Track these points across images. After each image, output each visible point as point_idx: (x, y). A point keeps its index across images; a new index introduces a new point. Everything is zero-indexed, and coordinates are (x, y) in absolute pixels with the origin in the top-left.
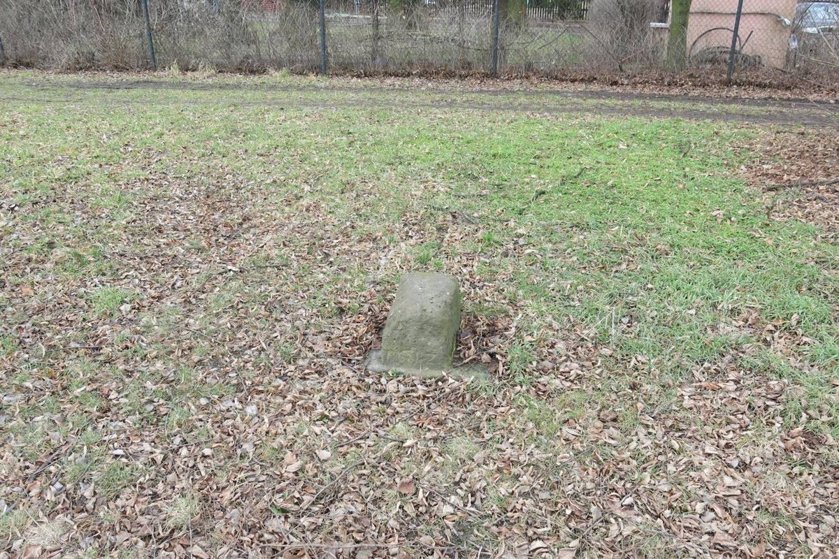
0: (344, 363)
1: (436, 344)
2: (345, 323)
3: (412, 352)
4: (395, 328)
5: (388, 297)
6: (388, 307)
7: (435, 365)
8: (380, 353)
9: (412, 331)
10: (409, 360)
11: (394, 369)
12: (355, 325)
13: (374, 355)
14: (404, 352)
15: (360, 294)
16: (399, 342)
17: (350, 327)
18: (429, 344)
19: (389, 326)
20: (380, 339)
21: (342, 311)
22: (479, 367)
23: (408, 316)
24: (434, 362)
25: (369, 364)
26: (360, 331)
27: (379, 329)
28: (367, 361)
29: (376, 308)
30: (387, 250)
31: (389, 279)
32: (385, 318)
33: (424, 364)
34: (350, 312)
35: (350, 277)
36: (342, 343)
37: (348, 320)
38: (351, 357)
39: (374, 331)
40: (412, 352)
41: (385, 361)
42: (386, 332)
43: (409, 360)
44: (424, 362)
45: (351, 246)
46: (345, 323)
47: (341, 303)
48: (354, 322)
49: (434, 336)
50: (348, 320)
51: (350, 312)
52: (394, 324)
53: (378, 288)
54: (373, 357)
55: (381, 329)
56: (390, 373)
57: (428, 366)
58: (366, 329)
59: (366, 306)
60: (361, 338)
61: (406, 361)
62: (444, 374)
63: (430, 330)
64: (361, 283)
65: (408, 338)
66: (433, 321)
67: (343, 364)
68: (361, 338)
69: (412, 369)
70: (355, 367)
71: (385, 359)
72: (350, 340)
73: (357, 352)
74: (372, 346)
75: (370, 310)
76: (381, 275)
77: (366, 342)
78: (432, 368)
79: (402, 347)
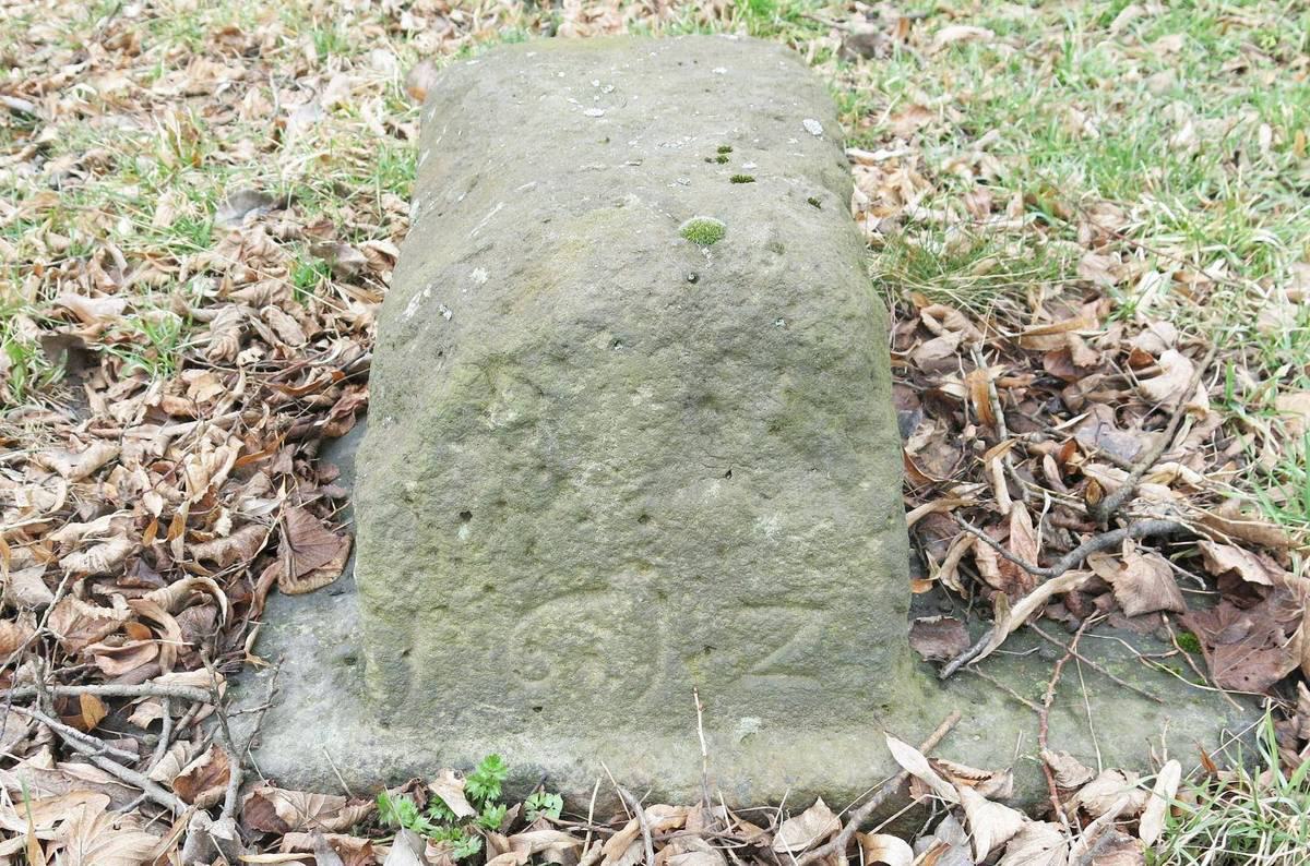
0: (70, 734)
1: (832, 521)
2: (105, 429)
3: (616, 603)
4: (460, 424)
5: (353, 256)
6: (358, 311)
7: (820, 689)
8: (349, 618)
9: (623, 410)
10: (595, 673)
11: (473, 747)
12: (158, 436)
13: (300, 637)
14: (548, 612)
15: (185, 261)
16: (504, 535)
17: (131, 450)
18: (770, 523)
19: (399, 409)
20: (331, 510)
21: (82, 360)
22: (1117, 654)
23: (574, 296)
24: (807, 666)
25: (270, 716)
26: (194, 472)
27: (312, 430)
28: (251, 698)
29: (288, 326)
30: (311, 80)
31: (343, 175)
32: (357, 377)
33: (717, 700)
34: (133, 364)
35: (132, 191)
36: (52, 576)
37: (122, 410)
38: (123, 677)
39: (285, 463)
40: (616, 603)
41: (399, 699)
42: (379, 462)
43: (595, 673)
44: (725, 679)
45: (146, 82)
46: (105, 429)
47: (76, 319)
48: (155, 415)
49: (812, 451)
50: (122, 410)
51: (133, 364)
52: (442, 387)
53: (287, 222)
54: (299, 662)
55: (327, 443)
56: (450, 791)
57: (754, 703)
58: (230, 451)
59: (223, 330)
60: (199, 521)
61: (573, 681)
62: (913, 761)
63: (770, 406)
64: (190, 209)
65: (582, 492)
66: (804, 318)
67: (61, 752)
68: (199, 521)
69: (623, 736)
70: (163, 765)
71: (398, 688)
72: (116, 548)
73: (175, 634)
74: (281, 567)
75: (248, 338)
76: (286, 171)
77: (239, 541)
78: (793, 714)
79: (534, 570)
